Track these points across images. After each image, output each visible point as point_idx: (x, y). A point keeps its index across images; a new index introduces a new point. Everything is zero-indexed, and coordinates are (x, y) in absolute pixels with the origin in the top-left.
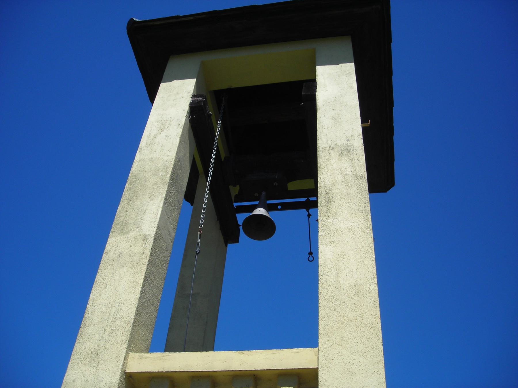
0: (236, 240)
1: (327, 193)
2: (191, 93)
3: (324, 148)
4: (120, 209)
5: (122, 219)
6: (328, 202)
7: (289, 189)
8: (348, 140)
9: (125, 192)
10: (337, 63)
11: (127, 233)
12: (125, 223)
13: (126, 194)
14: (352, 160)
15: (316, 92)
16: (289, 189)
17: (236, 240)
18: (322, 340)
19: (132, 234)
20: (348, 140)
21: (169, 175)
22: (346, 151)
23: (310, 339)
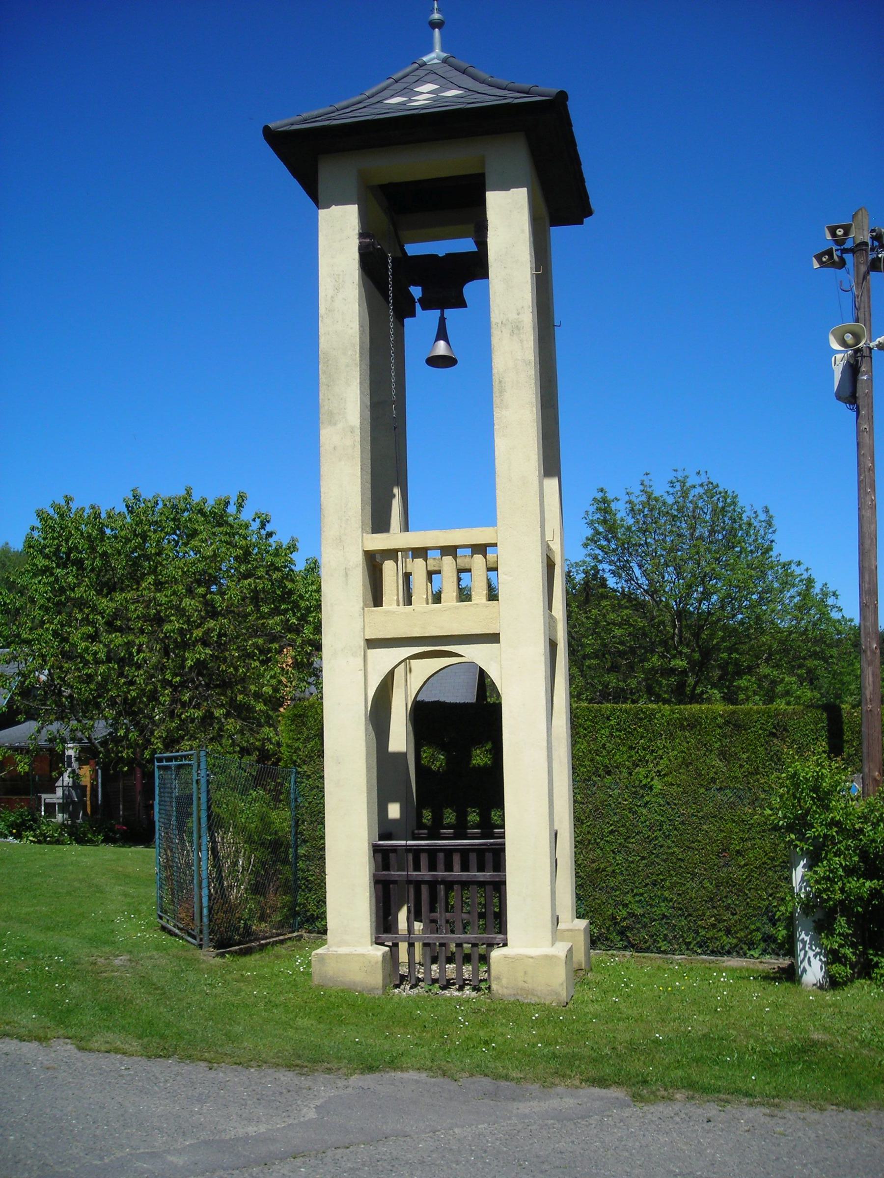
0: (413, 314)
1: (500, 382)
2: (357, 231)
3: (497, 324)
4: (321, 396)
5: (326, 407)
6: (502, 392)
7: (420, 288)
8: (518, 314)
9: (321, 376)
10: (507, 189)
11: (335, 424)
12: (331, 413)
13: (323, 378)
14: (521, 341)
15: (486, 237)
16: (420, 288)
17: (413, 314)
18: (499, 524)
19: (340, 426)
20: (518, 314)
21: (358, 355)
22: (516, 328)
23: (491, 520)
